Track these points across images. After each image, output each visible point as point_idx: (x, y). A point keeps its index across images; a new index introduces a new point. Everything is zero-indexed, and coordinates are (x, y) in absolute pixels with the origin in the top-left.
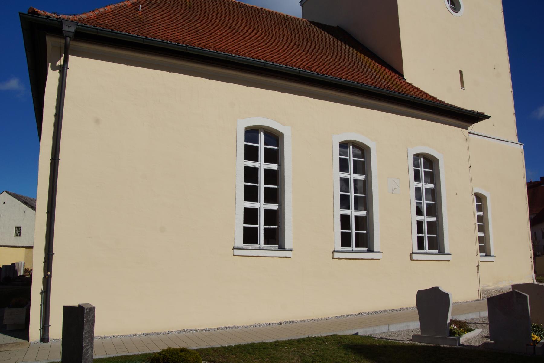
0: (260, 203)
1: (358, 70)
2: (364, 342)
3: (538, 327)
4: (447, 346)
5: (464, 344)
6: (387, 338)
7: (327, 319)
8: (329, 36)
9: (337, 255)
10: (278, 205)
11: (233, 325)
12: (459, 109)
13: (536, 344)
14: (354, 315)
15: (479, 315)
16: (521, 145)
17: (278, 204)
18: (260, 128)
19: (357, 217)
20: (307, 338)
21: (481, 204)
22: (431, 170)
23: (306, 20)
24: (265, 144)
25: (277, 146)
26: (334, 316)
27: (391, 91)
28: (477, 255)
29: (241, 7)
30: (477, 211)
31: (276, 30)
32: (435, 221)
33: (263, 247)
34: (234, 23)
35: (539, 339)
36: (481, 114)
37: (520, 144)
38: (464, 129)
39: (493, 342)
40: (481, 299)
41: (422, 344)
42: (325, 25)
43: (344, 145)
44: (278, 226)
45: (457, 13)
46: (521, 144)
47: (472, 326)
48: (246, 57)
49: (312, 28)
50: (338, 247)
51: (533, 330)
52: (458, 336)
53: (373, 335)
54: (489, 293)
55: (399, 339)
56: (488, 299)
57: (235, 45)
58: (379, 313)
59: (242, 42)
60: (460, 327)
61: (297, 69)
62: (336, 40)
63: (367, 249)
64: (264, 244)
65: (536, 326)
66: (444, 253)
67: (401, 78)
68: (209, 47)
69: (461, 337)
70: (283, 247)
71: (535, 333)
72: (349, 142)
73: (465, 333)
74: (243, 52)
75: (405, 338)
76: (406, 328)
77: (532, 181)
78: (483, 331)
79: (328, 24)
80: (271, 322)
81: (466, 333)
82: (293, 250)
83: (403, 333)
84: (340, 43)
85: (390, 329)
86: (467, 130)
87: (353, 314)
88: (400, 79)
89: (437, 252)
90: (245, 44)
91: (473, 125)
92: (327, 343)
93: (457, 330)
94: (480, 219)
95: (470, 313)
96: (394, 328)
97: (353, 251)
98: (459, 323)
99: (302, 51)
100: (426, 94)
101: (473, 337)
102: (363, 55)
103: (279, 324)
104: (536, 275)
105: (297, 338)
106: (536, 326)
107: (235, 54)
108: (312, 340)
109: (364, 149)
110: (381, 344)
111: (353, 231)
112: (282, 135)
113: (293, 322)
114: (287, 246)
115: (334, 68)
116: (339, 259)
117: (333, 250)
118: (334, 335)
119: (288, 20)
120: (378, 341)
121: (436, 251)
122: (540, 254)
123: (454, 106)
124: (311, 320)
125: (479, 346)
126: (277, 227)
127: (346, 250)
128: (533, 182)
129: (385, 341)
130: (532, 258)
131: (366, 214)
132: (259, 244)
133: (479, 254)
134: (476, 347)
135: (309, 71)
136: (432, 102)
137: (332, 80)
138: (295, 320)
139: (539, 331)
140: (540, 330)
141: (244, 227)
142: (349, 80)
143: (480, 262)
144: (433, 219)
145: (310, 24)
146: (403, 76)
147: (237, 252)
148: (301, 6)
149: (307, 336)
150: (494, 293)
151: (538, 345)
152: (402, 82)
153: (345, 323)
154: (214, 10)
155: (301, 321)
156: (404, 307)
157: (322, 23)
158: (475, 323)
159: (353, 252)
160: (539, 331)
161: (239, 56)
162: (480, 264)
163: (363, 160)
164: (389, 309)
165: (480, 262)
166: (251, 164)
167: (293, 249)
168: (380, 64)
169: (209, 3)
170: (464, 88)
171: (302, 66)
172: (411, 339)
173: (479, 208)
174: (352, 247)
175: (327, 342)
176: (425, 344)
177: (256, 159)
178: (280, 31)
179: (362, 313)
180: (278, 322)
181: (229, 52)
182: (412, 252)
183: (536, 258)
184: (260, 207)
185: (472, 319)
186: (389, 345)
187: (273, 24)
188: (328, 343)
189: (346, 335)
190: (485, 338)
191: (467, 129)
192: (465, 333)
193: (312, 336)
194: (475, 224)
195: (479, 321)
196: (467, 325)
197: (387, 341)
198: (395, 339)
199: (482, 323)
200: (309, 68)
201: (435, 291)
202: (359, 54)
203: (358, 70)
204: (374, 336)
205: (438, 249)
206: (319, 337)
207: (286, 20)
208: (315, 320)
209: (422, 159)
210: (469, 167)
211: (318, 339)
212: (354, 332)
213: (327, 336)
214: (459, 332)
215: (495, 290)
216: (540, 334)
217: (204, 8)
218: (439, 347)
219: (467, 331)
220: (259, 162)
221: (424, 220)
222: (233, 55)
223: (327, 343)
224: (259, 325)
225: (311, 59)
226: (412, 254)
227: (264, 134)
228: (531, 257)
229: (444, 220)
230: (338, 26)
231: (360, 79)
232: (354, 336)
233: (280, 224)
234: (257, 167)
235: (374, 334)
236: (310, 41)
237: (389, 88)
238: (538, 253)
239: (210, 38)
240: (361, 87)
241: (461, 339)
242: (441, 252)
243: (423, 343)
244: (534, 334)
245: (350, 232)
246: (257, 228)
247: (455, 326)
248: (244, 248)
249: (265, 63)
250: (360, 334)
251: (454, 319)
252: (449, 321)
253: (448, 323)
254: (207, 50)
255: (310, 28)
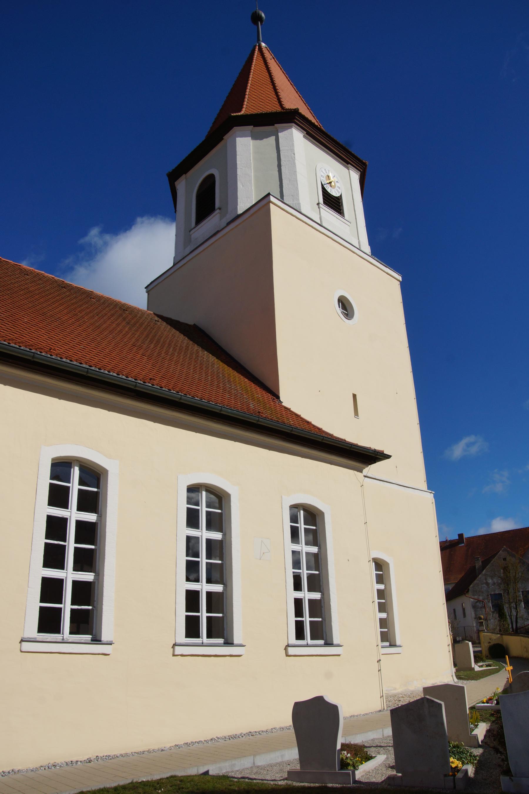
0: (67, 570)
1: (218, 387)
2: (217, 786)
3: (458, 747)
4: (337, 785)
5: (361, 781)
6: (251, 777)
7: (162, 750)
8: (182, 336)
9: (179, 650)
10: (94, 574)
11: (12, 769)
12: (351, 445)
13: (456, 773)
14: (203, 741)
15: (382, 733)
16: (431, 494)
17: (94, 573)
18: (74, 460)
19: (209, 594)
20: (129, 784)
21: (381, 573)
22: (314, 528)
23: (152, 312)
24: (81, 483)
25: (98, 487)
26: (173, 744)
27: (261, 418)
28: (377, 646)
29: (62, 287)
30: (377, 583)
31: (108, 323)
32: (319, 598)
33: (68, 638)
34: (50, 308)
35: (460, 765)
36: (380, 453)
37: (430, 493)
38: (358, 471)
39: (400, 775)
40: (384, 709)
41: (302, 784)
42: (178, 322)
43: (193, 489)
44: (93, 606)
45: (350, 321)
46: (430, 491)
47: (371, 752)
48: (61, 358)
49: (159, 323)
50: (181, 637)
51: (453, 752)
52: (352, 768)
53: (230, 774)
54: (395, 699)
55: (268, 778)
56: (392, 711)
57: (47, 339)
58: (241, 737)
59: (58, 336)
60: (355, 754)
61: (134, 380)
62: (191, 342)
63: (224, 640)
64: (71, 633)
65: (456, 745)
66: (333, 644)
67: (276, 400)
68: (9, 340)
69: (357, 770)
70: (98, 639)
71: (455, 756)
72: (201, 486)
73: (362, 764)
74: (58, 350)
75: (278, 776)
76: (279, 760)
77: (449, 539)
78: (387, 758)
79: (182, 320)
80: (74, 759)
81: (364, 762)
82: (114, 644)
83: (275, 768)
84: (196, 347)
85: (255, 762)
86: (362, 473)
87: (203, 740)
88: (274, 400)
89: (323, 643)
90: (63, 339)
91: (369, 466)
92: (160, 791)
93: (351, 760)
94: (381, 594)
95: (370, 731)
96: (262, 760)
97: (203, 643)
98: (355, 748)
99: (142, 355)
100: (308, 423)
101: (373, 768)
102: (226, 366)
103: (87, 763)
104: (456, 669)
105: (114, 785)
106: (456, 745)
107: (46, 353)
108: (137, 787)
109: (222, 496)
110: (242, 788)
111: (204, 615)
112: (106, 472)
113: (110, 757)
114: (105, 637)
115: (185, 381)
116: (182, 655)
117: (174, 643)
118: (172, 777)
119: (126, 310)
120: (238, 784)
121: (322, 642)
122: (461, 639)
123: (345, 441)
124: (138, 753)
125: (382, 782)
126: (90, 607)
127: (192, 643)
128: (449, 541)
129: (247, 782)
130: (450, 646)
131: (222, 589)
132: (61, 633)
133: (381, 644)
134: (377, 783)
135: (150, 385)
136: (316, 434)
137: (181, 399)
138: (112, 753)
139: (460, 752)
140: (462, 752)
141: (41, 608)
142: (205, 400)
143: (382, 654)
144: (316, 596)
145: (156, 318)
146: (278, 397)
147: (26, 646)
148: (147, 292)
149: (130, 781)
150: (403, 698)
151: (458, 774)
152: (277, 405)
153: (190, 756)
154: (23, 288)
155: (122, 755)
156: (278, 727)
157: (173, 318)
158: (377, 746)
159: (202, 645)
160: (460, 753)
161: (51, 355)
162: (383, 658)
163: (220, 511)
164: (256, 730)
165: (382, 654)
166: (58, 512)
167: (113, 642)
168: (249, 379)
169: (17, 276)
170: (358, 417)
171: (141, 378)
172: (287, 776)
173: (380, 579)
174: (202, 638)
175: (160, 789)
176: (306, 784)
177: (64, 504)
178: (114, 325)
179: (216, 739)
180: (85, 758)
181: (38, 350)
182: (288, 644)
183: (456, 645)
184: (66, 578)
185: (373, 740)
186: (254, 789)
187: (106, 314)
188: (161, 790)
189: (189, 776)
190: (390, 769)
191: (361, 472)
192: (362, 763)
193: (137, 780)
194: (374, 601)
195: (382, 742)
196: (365, 750)
197: (251, 783)
198: (263, 778)
199: (386, 745)
200: (151, 379)
201: (319, 700)
202: (221, 363)
203: (218, 387)
204: (233, 774)
205: (325, 639)
206: (148, 781)
207: (124, 310)
208: (143, 752)
209: (302, 512)
210: (365, 524)
211: (147, 785)
212: (202, 770)
213: (160, 779)
214: (353, 762)
215: (404, 695)
216: (462, 758)
217: (9, 283)
218: (326, 787)
219: (366, 758)
220: (69, 510)
221: (304, 597)
222: (43, 354)
223: (160, 791)
224: (55, 766)
225: (154, 368)
226: (287, 647)
227: (80, 470)
228: (448, 646)
229: (331, 598)
230: (194, 324)
231: (220, 398)
232: (202, 776)
233: (95, 602)
234: (65, 517)
235: (232, 772)
236: (154, 342)
237: (259, 412)
238: (459, 637)
239: (13, 327)
240: (221, 410)
241: (357, 772)
242: (329, 643)
243: (303, 782)
244: (454, 759)
245: (199, 616)
246: (60, 609)
247: (347, 753)
248: (38, 640)
249: (88, 369)
250: (211, 773)
251: (347, 742)
252: (339, 747)
253: (338, 750)
254: (5, 343)
255: (156, 324)
